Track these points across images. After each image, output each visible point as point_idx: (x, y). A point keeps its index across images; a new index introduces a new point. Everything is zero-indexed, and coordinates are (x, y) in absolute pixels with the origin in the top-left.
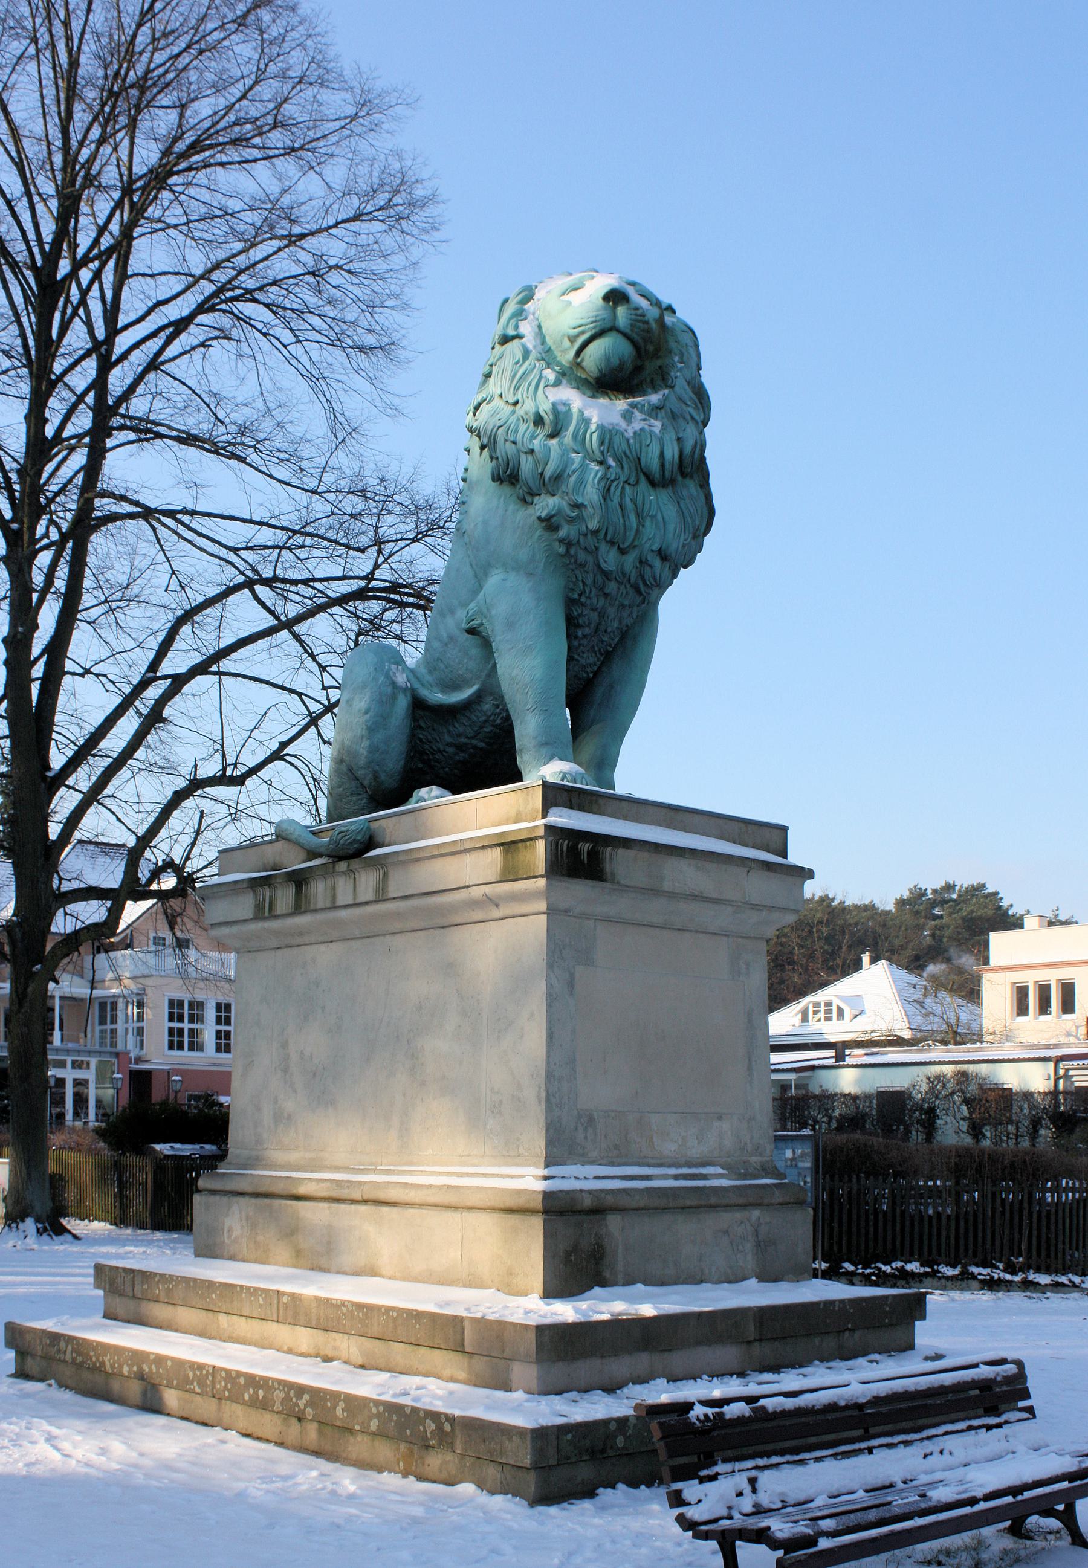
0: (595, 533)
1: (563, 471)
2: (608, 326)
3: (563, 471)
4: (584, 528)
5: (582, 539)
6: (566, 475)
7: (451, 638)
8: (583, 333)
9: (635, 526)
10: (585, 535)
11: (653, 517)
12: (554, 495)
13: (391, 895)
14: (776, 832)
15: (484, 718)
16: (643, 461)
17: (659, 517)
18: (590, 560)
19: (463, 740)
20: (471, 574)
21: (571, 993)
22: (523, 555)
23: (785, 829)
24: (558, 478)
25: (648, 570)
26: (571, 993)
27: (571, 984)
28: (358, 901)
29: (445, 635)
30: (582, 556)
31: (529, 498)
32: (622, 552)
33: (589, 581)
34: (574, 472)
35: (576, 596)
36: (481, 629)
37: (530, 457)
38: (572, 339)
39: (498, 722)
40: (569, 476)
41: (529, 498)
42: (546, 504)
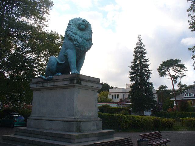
7: (62, 56)
23: (100, 79)
42: (75, 43)
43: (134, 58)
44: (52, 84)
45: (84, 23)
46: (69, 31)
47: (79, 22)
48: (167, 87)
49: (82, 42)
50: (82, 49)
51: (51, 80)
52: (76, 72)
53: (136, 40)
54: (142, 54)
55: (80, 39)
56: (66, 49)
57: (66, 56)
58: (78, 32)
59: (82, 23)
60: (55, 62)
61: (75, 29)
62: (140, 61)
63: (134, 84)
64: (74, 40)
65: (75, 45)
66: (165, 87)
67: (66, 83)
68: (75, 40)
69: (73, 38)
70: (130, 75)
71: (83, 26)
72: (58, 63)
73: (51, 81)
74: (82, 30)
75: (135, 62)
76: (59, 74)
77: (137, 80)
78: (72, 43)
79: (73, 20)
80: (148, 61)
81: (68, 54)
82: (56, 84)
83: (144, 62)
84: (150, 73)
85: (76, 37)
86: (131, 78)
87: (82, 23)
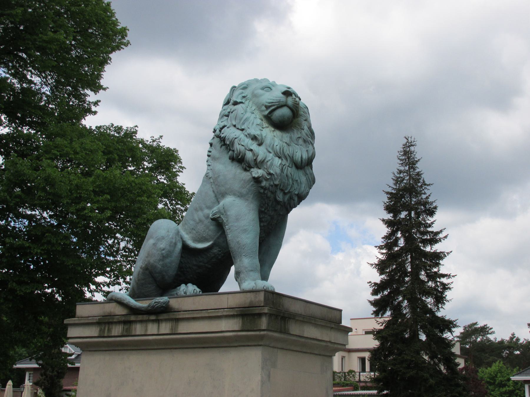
0: (276, 186)
1: (265, 160)
2: (284, 104)
3: (265, 160)
4: (272, 183)
5: (270, 187)
6: (266, 161)
7: (200, 221)
8: (274, 105)
9: (291, 184)
10: (272, 186)
11: (297, 181)
12: (260, 169)
13: (179, 332)
14: (338, 312)
15: (213, 255)
16: (294, 158)
17: (299, 181)
18: (272, 196)
19: (201, 264)
20: (212, 195)
21: (269, 381)
22: (244, 191)
23: (340, 311)
24: (263, 162)
25: (292, 201)
26: (269, 381)
27: (269, 376)
28: (160, 333)
29: (197, 219)
30: (269, 194)
31: (248, 169)
32: (285, 194)
33: (270, 204)
34: (269, 160)
35: (263, 210)
36: (219, 219)
37: (250, 152)
38: (267, 107)
39: (220, 257)
40: (267, 162)
41: (248, 169)
42: (257, 172)
43: (385, 230)
44: (165, 328)
45: (290, 101)
46: (233, 129)
47: (268, 97)
48: (493, 333)
49: (282, 170)
50: (280, 197)
51: (160, 313)
52: (261, 284)
53: (394, 165)
54: (418, 215)
55: (277, 162)
56: (219, 195)
57: (218, 223)
58: (270, 134)
59: (283, 98)
60: (175, 244)
61: (255, 123)
62: (409, 239)
63: (389, 324)
64: (252, 164)
65: (257, 180)
66: (484, 330)
67: (228, 326)
68: (258, 164)
69: (249, 155)
70: (375, 293)
71: (285, 112)
72: (185, 248)
73: (161, 317)
74: (281, 125)
75: (389, 243)
76: (191, 288)
77: (397, 310)
78: (246, 176)
79: (245, 88)
80: (441, 236)
81: (227, 216)
82: (184, 328)
83: (426, 242)
84: (445, 287)
85: (261, 152)
86: (374, 303)
87: (283, 98)
